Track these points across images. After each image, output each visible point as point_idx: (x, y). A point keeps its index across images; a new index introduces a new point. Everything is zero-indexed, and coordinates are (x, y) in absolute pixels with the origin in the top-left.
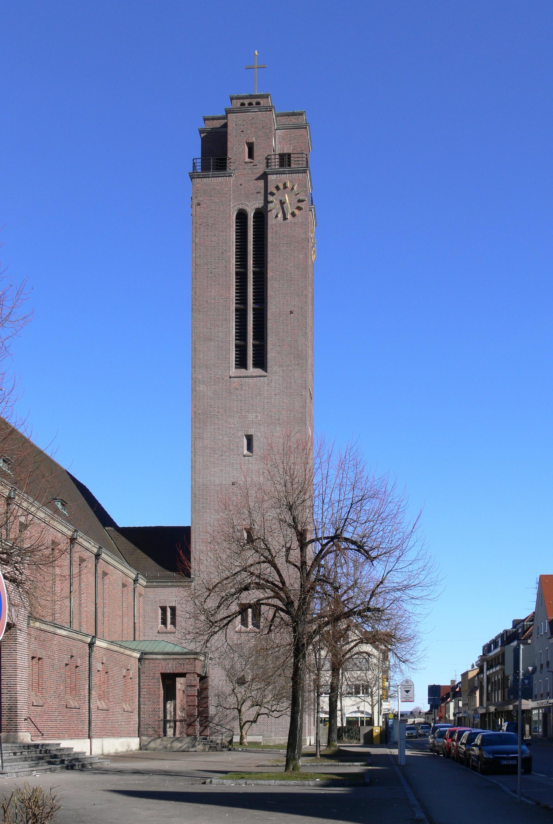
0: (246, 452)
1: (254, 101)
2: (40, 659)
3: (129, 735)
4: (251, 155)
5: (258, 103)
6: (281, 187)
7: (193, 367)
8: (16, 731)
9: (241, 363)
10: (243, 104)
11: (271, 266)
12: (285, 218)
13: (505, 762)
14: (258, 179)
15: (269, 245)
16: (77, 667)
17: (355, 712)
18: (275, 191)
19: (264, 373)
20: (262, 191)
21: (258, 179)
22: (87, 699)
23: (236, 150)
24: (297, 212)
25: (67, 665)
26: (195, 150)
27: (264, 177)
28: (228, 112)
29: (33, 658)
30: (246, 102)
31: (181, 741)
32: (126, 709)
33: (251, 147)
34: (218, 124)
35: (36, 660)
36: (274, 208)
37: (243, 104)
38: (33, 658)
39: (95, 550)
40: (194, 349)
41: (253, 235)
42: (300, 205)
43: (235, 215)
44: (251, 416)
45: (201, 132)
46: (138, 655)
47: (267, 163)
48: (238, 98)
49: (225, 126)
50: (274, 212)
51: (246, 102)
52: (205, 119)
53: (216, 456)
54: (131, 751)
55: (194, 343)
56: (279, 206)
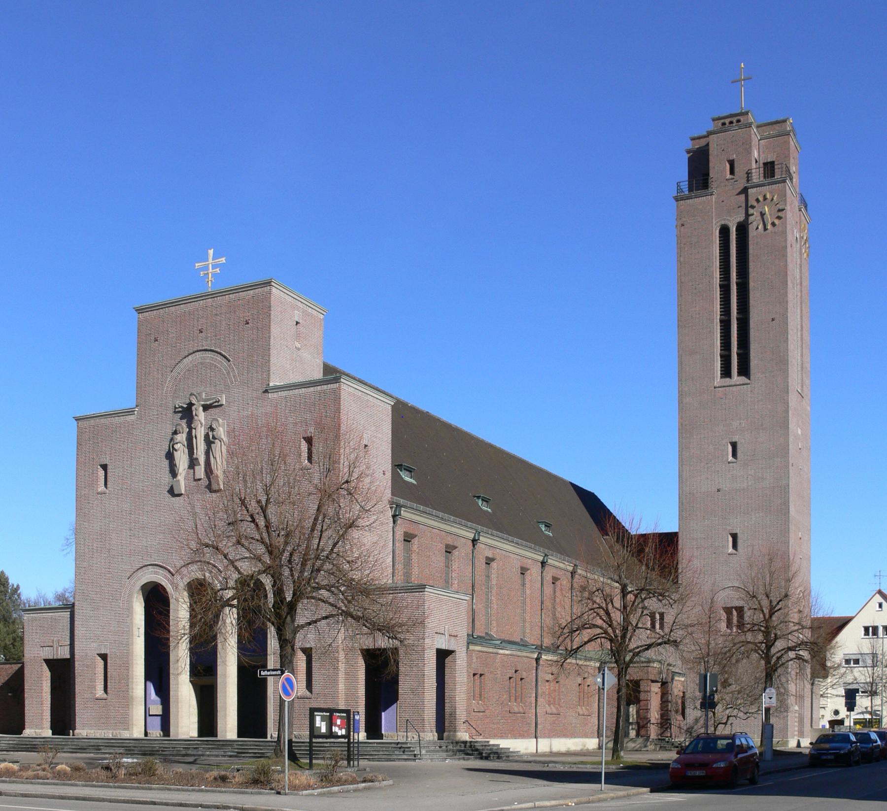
0: (730, 458)
1: (734, 120)
2: (481, 675)
3: (586, 736)
4: (732, 172)
5: (738, 121)
6: (761, 199)
7: (680, 380)
8: (455, 731)
9: (726, 372)
10: (724, 124)
11: (753, 275)
12: (765, 229)
13: (825, 757)
14: (739, 194)
15: (750, 256)
16: (522, 679)
17: (863, 713)
18: (755, 204)
19: (747, 381)
20: (744, 205)
21: (739, 194)
22: (534, 705)
23: (718, 168)
24: (776, 222)
25: (510, 678)
26: (682, 173)
27: (745, 191)
28: (710, 133)
29: (474, 675)
30: (727, 121)
31: (635, 742)
32: (581, 713)
33: (732, 163)
34: (703, 142)
35: (477, 677)
36: (755, 220)
37: (724, 124)
38: (474, 675)
39: (570, 569)
40: (681, 363)
41: (737, 250)
42: (780, 214)
43: (718, 232)
44: (735, 424)
45: (688, 152)
46: (598, 665)
47: (748, 177)
48: (719, 119)
49: (708, 145)
50: (755, 224)
51: (727, 121)
52: (693, 139)
53: (702, 464)
54: (588, 749)
55: (680, 357)
56: (759, 218)
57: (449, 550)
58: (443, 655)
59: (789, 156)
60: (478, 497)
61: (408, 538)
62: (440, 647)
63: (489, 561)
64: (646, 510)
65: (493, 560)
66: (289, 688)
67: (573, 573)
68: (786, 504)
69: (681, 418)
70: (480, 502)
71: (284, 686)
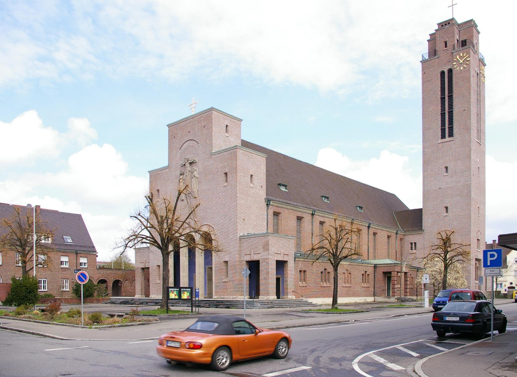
2: (304, 271)
9: (443, 136)
29: (300, 271)
35: (302, 272)
57: (299, 219)
58: (281, 265)
59: (473, 36)
60: (323, 197)
61: (375, 234)
62: (278, 259)
63: (322, 223)
64: (412, 199)
65: (324, 222)
66: (83, 278)
67: (397, 233)
68: (470, 192)
69: (423, 158)
70: (324, 198)
71: (79, 277)
